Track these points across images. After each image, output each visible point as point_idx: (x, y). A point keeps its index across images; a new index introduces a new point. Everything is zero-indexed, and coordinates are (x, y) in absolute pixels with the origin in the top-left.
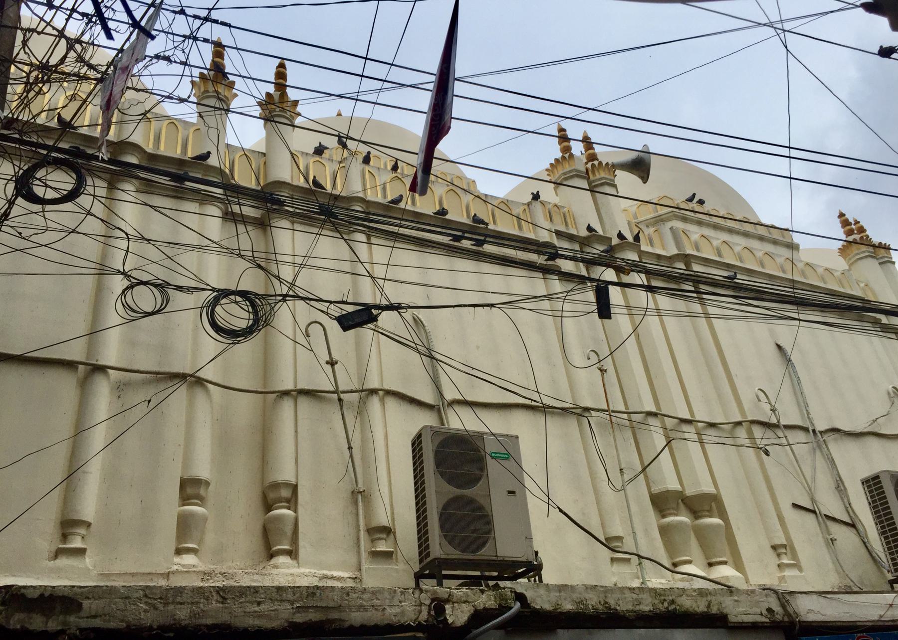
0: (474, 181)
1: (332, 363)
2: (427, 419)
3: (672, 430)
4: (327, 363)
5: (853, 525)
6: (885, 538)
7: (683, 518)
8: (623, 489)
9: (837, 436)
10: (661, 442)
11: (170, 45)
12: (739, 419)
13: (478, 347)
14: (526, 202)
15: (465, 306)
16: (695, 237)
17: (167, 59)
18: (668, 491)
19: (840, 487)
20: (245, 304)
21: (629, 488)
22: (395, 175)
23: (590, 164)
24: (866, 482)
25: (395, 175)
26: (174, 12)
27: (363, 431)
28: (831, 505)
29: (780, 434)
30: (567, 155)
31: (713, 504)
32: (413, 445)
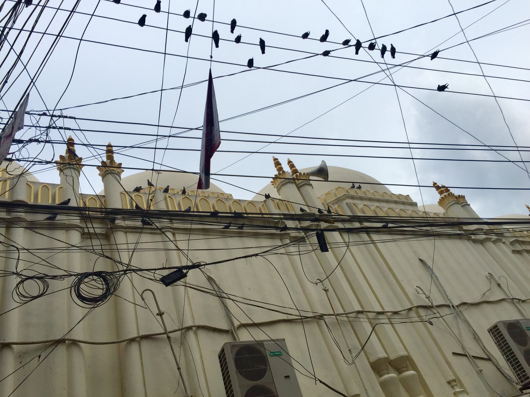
0: (231, 195)
1: (161, 314)
2: (224, 339)
3: (373, 319)
4: (158, 314)
5: (489, 359)
6: (511, 363)
7: (393, 375)
8: (354, 363)
9: (466, 307)
10: (369, 329)
11: (38, 133)
12: (410, 306)
13: (250, 289)
14: (263, 201)
15: (240, 258)
16: (361, 206)
17: (37, 141)
18: (380, 359)
19: (476, 338)
20: (100, 280)
21: (356, 361)
22: (184, 196)
23: (294, 176)
24: (490, 331)
25: (184, 196)
26: (39, 115)
27: (186, 355)
28: (474, 350)
29: (435, 311)
30: (281, 172)
31: (407, 362)
32: (219, 357)
